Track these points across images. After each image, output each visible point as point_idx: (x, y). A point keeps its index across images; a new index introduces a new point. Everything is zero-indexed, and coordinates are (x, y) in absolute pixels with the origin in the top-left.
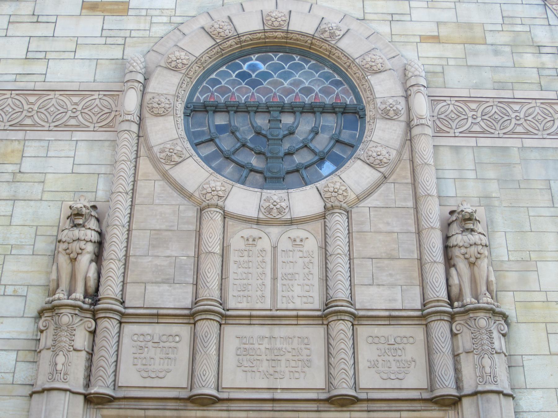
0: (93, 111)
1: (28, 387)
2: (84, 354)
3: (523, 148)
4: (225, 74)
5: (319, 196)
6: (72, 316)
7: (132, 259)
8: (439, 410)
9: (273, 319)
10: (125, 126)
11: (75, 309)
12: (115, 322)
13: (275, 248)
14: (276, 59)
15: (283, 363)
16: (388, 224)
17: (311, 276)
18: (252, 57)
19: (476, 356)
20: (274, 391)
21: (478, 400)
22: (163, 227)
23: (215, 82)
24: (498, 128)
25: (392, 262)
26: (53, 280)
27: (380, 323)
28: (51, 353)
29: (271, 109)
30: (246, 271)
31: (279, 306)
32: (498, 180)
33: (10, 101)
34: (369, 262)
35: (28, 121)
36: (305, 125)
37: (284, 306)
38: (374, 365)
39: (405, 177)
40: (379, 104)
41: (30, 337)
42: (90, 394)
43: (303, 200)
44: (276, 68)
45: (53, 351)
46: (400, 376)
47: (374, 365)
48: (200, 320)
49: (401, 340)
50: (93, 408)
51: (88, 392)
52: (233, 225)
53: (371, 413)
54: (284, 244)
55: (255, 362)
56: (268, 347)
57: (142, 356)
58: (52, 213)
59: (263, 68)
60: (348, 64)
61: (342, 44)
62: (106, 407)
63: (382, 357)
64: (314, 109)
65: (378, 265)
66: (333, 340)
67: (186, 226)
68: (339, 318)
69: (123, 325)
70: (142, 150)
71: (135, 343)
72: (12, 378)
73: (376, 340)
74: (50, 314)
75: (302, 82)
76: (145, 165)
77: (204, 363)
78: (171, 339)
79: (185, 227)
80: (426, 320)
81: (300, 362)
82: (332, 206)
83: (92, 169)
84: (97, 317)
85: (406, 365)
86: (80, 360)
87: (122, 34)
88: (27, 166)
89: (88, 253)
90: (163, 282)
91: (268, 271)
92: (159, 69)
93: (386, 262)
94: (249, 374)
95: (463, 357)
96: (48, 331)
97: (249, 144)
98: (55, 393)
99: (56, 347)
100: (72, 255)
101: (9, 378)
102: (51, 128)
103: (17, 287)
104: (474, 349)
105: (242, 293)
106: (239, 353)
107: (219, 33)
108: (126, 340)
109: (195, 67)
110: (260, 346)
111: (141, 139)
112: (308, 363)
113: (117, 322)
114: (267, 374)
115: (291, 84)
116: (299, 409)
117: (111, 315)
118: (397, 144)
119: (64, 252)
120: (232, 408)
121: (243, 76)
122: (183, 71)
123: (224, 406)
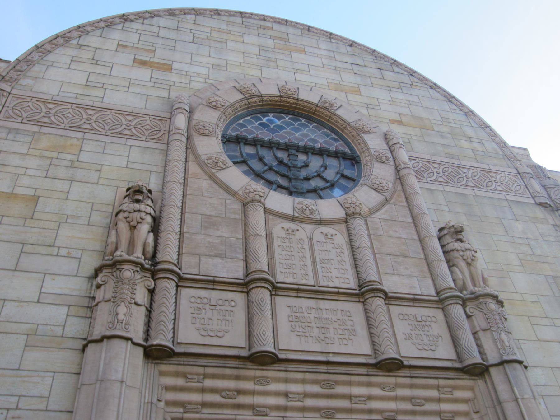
0: (145, 127)
1: (79, 341)
2: (143, 309)
3: (476, 196)
4: (249, 122)
5: (340, 206)
6: (134, 272)
7: (186, 235)
8: (469, 379)
9: (318, 293)
10: (177, 137)
11: (137, 267)
12: (174, 284)
13: (311, 239)
14: (287, 119)
15: (332, 330)
16: (396, 231)
17: (343, 263)
18: (269, 114)
19: (494, 333)
20: (327, 355)
21: (505, 369)
22: (213, 214)
23: (242, 126)
24: (456, 181)
25: (406, 259)
26: (112, 243)
27: (406, 304)
28: (112, 303)
29: (289, 147)
30: (289, 253)
31: (321, 283)
32: (465, 214)
33: (70, 110)
34: (388, 258)
35: (88, 126)
36: (315, 163)
37: (325, 284)
38: (409, 337)
39: (401, 202)
40: (373, 153)
41: (83, 294)
42: (152, 345)
43: (329, 207)
44: (289, 125)
45: (114, 302)
46: (433, 348)
47: (409, 337)
48: (255, 288)
49: (427, 319)
50: (152, 363)
51: (149, 343)
52: (273, 219)
53: (414, 380)
54: (318, 237)
55: (306, 328)
56: (316, 316)
57: (200, 316)
58: (109, 194)
59: (278, 123)
60: (344, 126)
61: (340, 112)
62: (162, 362)
63: (414, 331)
64: (321, 153)
65: (396, 260)
66: (373, 313)
67: (233, 215)
68: (376, 295)
69: (179, 289)
70: (191, 157)
71: (193, 305)
72: (62, 331)
73: (406, 317)
74: (110, 271)
75: (309, 136)
76: (193, 168)
77: (262, 324)
78: (227, 303)
79: (233, 216)
80: (442, 304)
81: (346, 331)
82: (353, 213)
83: (145, 167)
84: (155, 278)
85: (435, 339)
86: (140, 314)
87: (168, 83)
88: (84, 157)
89: (148, 223)
90: (216, 256)
91: (308, 255)
92: (201, 105)
93: (401, 259)
94: (303, 339)
95: (481, 334)
96: (107, 285)
97: (274, 168)
98: (116, 341)
99: (117, 298)
100: (132, 223)
101: (59, 331)
102: (107, 134)
103: (70, 250)
104: (491, 327)
105: (287, 270)
106: (291, 319)
107: (247, 90)
108: (184, 303)
109: (230, 110)
110: (309, 315)
111: (189, 150)
112: (353, 332)
113: (175, 284)
114: (319, 339)
115: (301, 135)
116: (351, 372)
117: (171, 276)
118: (392, 179)
119: (124, 220)
120: (290, 369)
121: (263, 125)
122: (222, 110)
123: (282, 366)
